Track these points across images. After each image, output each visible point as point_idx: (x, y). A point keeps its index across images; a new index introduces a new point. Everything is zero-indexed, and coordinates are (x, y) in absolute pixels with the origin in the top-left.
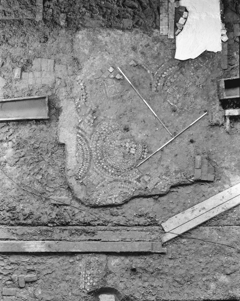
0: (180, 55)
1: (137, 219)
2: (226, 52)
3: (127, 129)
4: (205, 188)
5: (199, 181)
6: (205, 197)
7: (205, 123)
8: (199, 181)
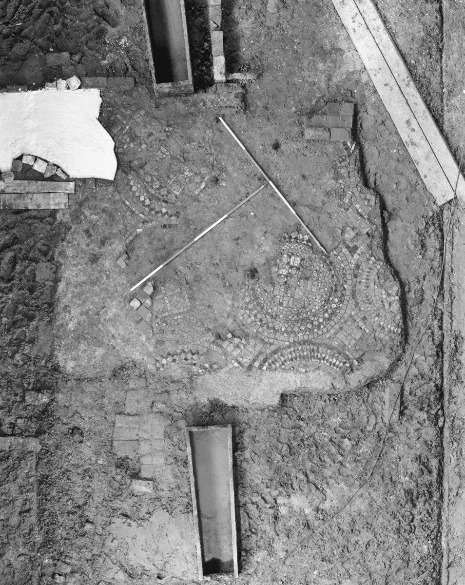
0: (105, 167)
1: (430, 253)
2: (102, 80)
3: (253, 273)
4: (368, 121)
5: (355, 133)
6: (385, 120)
7: (240, 120)
8: (355, 133)
